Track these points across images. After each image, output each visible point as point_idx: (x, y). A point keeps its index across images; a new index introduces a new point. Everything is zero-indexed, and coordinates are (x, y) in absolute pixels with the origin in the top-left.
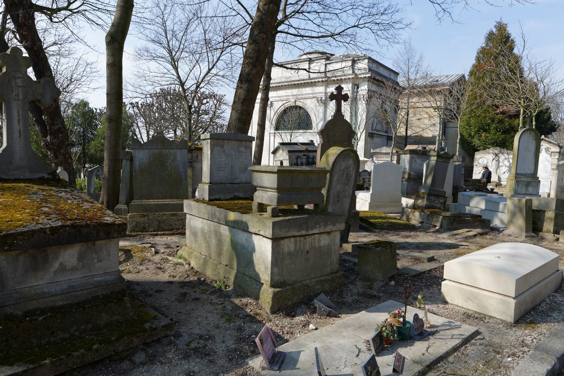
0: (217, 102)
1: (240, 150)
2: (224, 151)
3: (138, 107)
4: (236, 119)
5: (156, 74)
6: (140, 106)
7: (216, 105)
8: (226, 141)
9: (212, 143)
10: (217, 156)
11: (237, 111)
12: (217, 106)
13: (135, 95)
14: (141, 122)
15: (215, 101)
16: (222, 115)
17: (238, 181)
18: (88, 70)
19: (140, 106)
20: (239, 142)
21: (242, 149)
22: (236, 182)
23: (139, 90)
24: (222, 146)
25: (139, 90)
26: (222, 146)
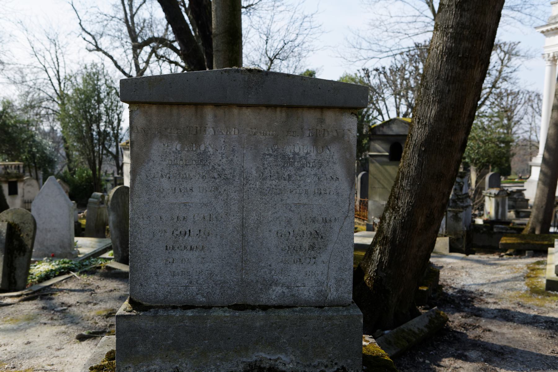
0: (505, 54)
1: (289, 150)
2: (203, 159)
3: (385, 73)
4: (442, 53)
5: (398, 19)
6: (388, 72)
7: (502, 61)
8: (209, 113)
9: (141, 121)
10: (165, 183)
11: (445, 32)
12: (505, 62)
13: (371, 54)
14: (387, 93)
15: (502, 54)
16: (513, 75)
17: (274, 295)
18: (306, 25)
19: (388, 72)
20: (280, 116)
21: (301, 147)
22: (263, 300)
23: (375, 47)
24: (192, 137)
25: (375, 47)
26: (192, 137)
